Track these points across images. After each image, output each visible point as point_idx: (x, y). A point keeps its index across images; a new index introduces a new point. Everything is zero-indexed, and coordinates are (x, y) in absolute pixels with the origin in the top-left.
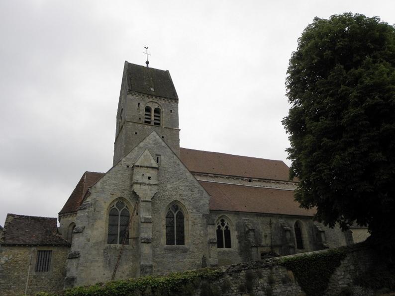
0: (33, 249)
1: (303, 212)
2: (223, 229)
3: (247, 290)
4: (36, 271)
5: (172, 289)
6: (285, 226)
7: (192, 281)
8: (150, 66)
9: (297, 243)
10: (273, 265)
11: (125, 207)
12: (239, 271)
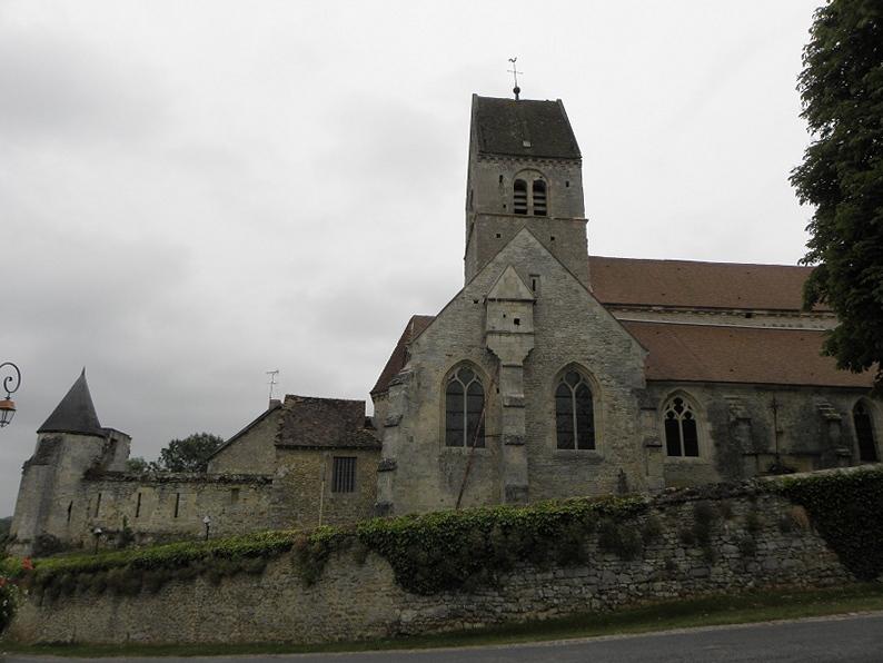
0: (326, 454)
1: (848, 378)
2: (680, 418)
3: (697, 541)
5: (541, 531)
6: (828, 411)
7: (580, 519)
8: (521, 97)
9: (861, 448)
10: (758, 493)
12: (680, 502)
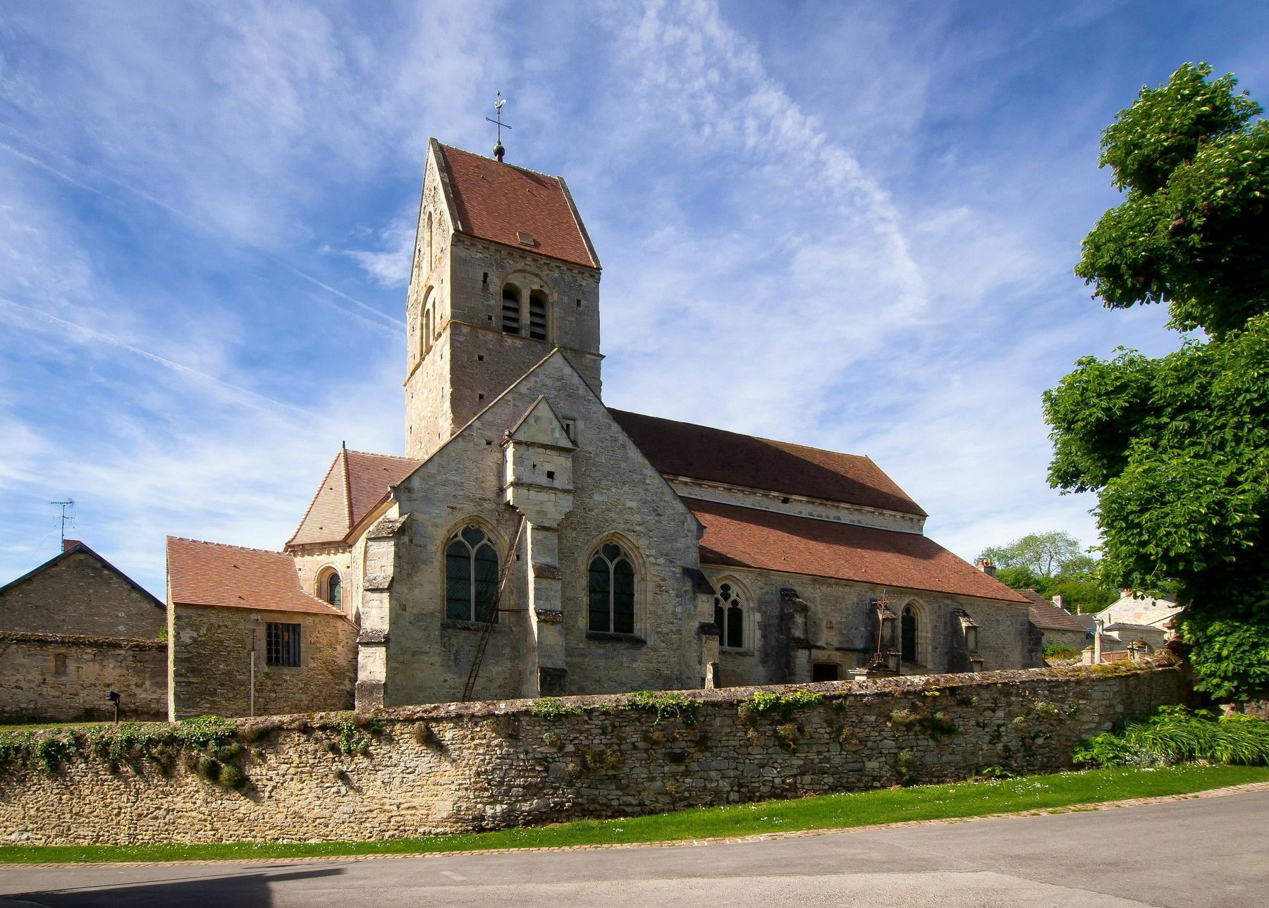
2: (726, 606)
4: (269, 661)
11: (485, 541)
